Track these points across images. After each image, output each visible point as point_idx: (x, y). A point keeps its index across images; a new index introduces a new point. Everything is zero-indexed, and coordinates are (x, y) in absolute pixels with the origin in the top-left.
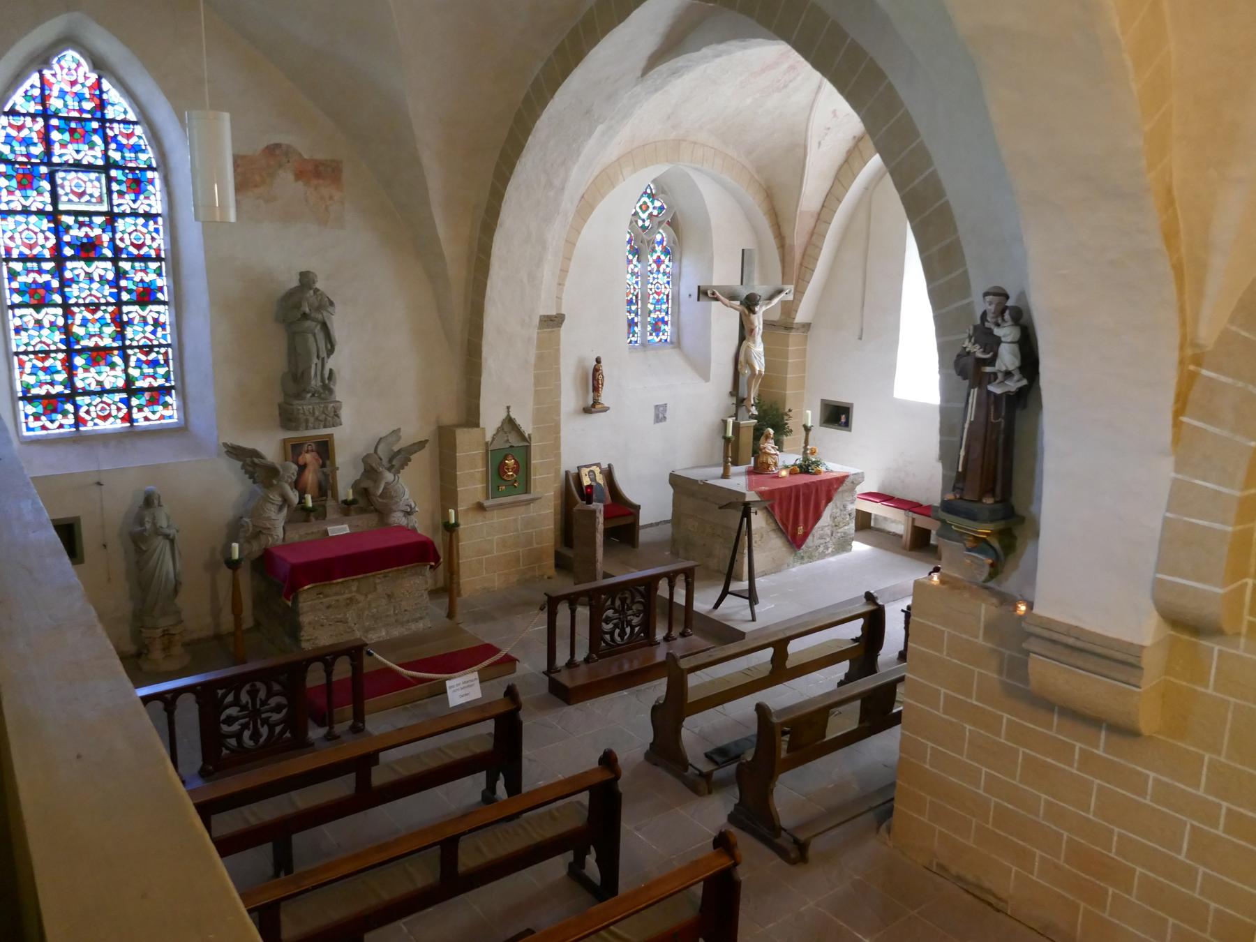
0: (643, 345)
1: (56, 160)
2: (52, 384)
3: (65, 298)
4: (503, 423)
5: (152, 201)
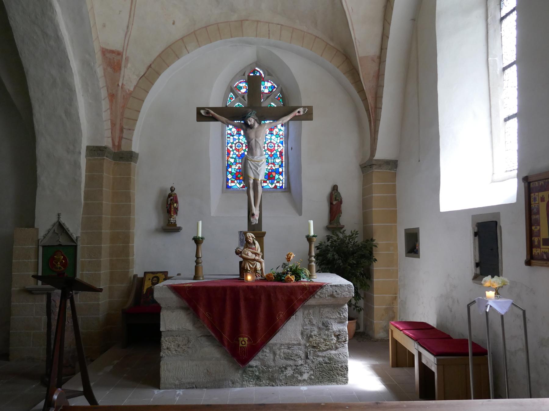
4: (54, 225)
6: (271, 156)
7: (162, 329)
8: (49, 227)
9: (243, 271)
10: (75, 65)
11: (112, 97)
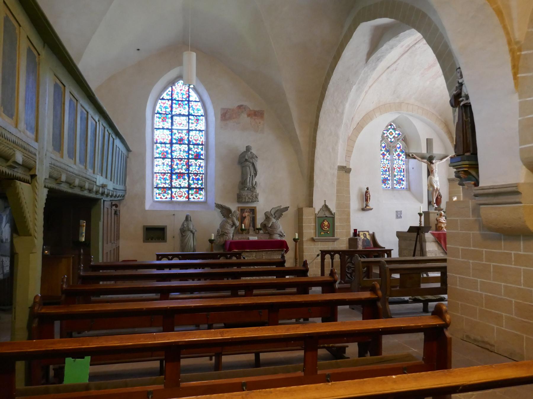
0: (392, 188)
1: (174, 113)
2: (165, 183)
3: (172, 156)
5: (202, 126)
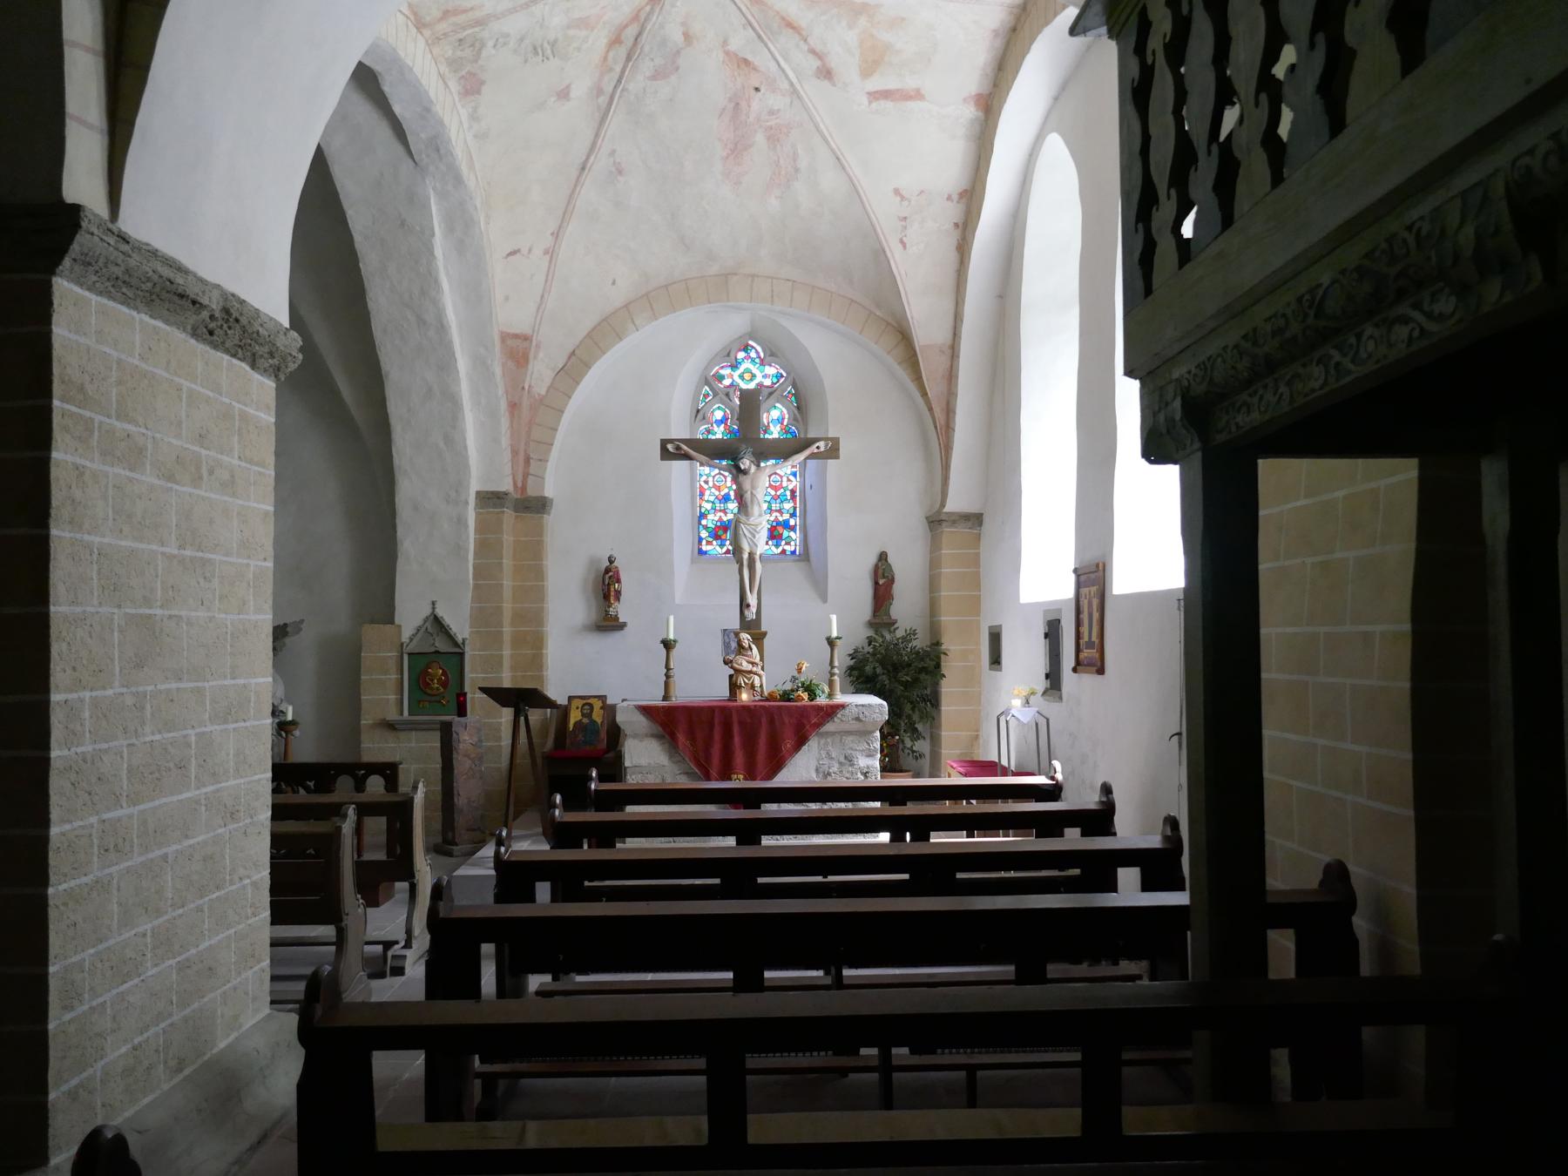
4: (426, 620)
6: (776, 498)
7: (627, 764)
8: (418, 621)
9: (734, 687)
10: (463, 364)
11: (513, 406)
